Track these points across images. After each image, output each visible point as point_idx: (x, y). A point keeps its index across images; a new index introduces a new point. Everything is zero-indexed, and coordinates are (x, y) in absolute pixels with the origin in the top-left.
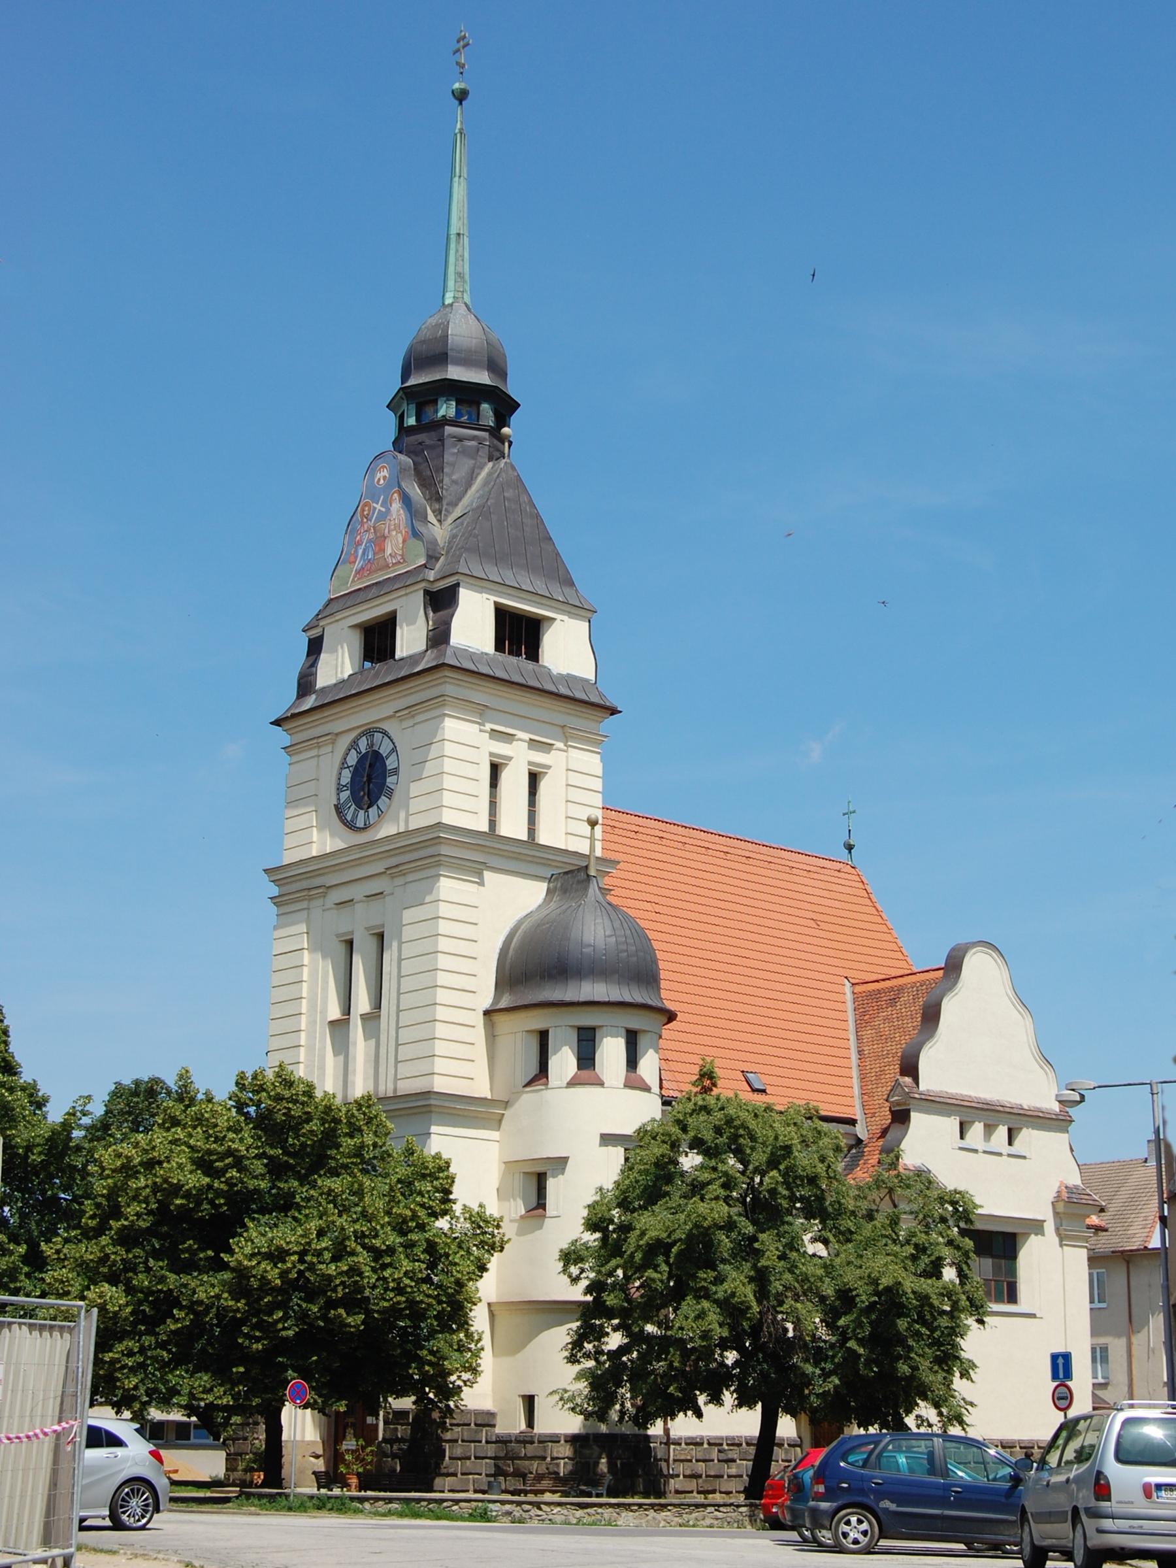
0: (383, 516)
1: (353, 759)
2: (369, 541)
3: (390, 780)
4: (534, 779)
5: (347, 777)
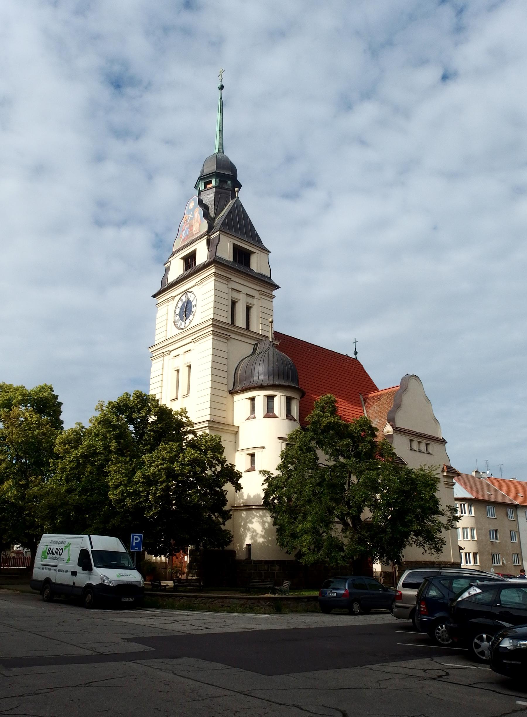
0: (192, 219)
1: (180, 304)
2: (187, 228)
3: (194, 309)
4: (248, 309)
5: (178, 311)
